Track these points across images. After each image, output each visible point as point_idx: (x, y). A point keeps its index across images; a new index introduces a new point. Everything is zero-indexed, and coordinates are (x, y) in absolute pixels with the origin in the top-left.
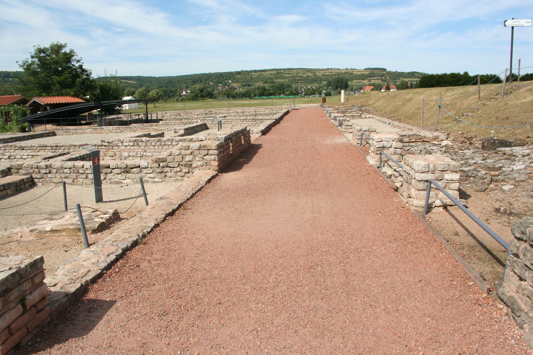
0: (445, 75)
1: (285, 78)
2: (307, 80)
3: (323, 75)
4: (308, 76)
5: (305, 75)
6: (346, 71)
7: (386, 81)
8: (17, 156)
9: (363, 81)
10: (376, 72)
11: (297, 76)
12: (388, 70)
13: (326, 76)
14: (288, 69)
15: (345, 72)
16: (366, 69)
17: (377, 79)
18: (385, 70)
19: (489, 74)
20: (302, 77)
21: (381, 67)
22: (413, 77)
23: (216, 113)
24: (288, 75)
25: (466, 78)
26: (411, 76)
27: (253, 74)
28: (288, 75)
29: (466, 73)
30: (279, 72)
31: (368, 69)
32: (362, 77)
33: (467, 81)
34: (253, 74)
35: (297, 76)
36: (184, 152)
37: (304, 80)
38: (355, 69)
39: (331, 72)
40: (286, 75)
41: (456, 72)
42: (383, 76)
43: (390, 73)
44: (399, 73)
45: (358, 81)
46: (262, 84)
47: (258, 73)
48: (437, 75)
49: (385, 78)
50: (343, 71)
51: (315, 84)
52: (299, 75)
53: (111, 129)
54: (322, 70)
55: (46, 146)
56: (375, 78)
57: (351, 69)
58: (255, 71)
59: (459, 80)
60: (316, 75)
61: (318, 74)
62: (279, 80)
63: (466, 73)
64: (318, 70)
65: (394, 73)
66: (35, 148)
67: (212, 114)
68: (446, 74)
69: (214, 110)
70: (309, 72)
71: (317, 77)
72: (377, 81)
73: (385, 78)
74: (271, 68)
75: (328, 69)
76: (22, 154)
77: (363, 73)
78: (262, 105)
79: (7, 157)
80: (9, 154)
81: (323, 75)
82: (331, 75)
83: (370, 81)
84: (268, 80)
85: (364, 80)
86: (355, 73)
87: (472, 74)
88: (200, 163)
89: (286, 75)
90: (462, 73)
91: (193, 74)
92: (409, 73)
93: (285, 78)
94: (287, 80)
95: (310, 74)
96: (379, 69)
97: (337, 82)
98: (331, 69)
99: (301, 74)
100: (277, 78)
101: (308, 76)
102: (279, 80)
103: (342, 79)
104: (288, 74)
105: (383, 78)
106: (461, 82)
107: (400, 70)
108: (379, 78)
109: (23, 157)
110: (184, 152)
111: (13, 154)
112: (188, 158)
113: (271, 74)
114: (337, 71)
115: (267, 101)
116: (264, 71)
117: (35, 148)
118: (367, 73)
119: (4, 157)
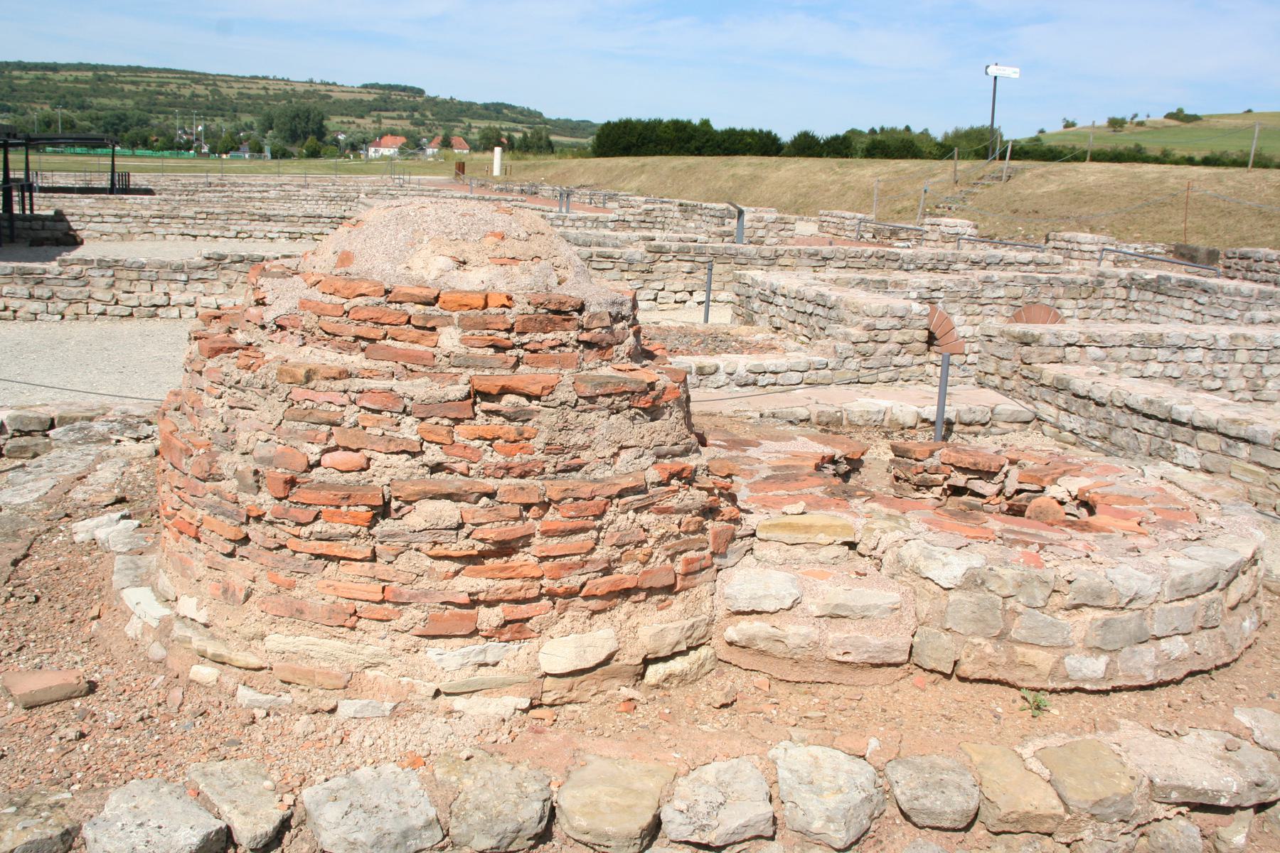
0: (659, 123)
1: (123, 95)
2: (190, 107)
3: (240, 94)
4: (194, 95)
5: (187, 92)
6: (307, 87)
7: (423, 124)
8: (256, 234)
9: (358, 121)
10: (394, 96)
11: (160, 93)
12: (430, 92)
13: (249, 97)
14: (130, 69)
15: (306, 91)
16: (365, 86)
17: (400, 118)
18: (420, 92)
19: (634, 118)
20: (176, 96)
21: (409, 84)
22: (497, 119)
23: (234, 184)
24: (133, 88)
25: (706, 133)
26: (494, 115)
27: (16, 73)
28: (133, 88)
29: (706, 123)
30: (103, 77)
31: (373, 86)
32: (357, 108)
33: (708, 141)
34: (16, 73)
35: (160, 93)
36: (756, 224)
37: (183, 105)
38: (334, 84)
39: (265, 88)
40: (127, 87)
41: (683, 117)
42: (414, 109)
43: (433, 102)
44: (461, 103)
45: (345, 119)
46: (47, 108)
47: (32, 74)
48: (639, 122)
49: (423, 115)
50: (300, 89)
51: (219, 120)
52: (168, 89)
53: (147, 202)
54: (238, 79)
55: (320, 217)
56: (394, 114)
57: (323, 83)
58: (21, 66)
59: (691, 138)
60: (220, 94)
61: (224, 91)
62: (105, 101)
63: (706, 123)
64: (227, 79)
65: (445, 102)
66: (295, 219)
67: (223, 185)
68: (660, 122)
69: (233, 178)
70: (197, 82)
71: (224, 99)
72: (398, 122)
73: (423, 115)
74: (74, 61)
75: (256, 77)
76: (268, 228)
77: (358, 97)
78: (162, 170)
79: (233, 234)
80: (239, 229)
81: (240, 94)
82: (267, 98)
83: (379, 121)
84: (69, 98)
85: (362, 117)
86: (336, 95)
87: (719, 125)
88: (775, 240)
89: (127, 87)
90: (696, 121)
91: (747, 126)
92: (486, 107)
93: (123, 95)
94: (130, 103)
95: (200, 89)
96: (404, 89)
97: (294, 118)
98: (265, 78)
99: (173, 87)
100: (96, 93)
101: (194, 95)
102: (105, 101)
103: (308, 111)
104: (133, 83)
105: (417, 115)
106: (694, 144)
107: (463, 96)
108: (405, 114)
109: (270, 235)
110: (756, 224)
111: (245, 228)
112: (761, 233)
113: (77, 80)
114: (282, 86)
115: (172, 162)
116: (55, 68)
117: (295, 219)
118: (371, 98)
119: (226, 234)
